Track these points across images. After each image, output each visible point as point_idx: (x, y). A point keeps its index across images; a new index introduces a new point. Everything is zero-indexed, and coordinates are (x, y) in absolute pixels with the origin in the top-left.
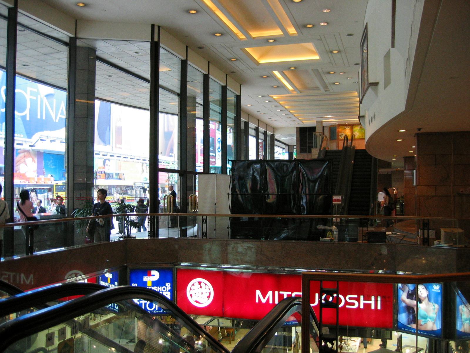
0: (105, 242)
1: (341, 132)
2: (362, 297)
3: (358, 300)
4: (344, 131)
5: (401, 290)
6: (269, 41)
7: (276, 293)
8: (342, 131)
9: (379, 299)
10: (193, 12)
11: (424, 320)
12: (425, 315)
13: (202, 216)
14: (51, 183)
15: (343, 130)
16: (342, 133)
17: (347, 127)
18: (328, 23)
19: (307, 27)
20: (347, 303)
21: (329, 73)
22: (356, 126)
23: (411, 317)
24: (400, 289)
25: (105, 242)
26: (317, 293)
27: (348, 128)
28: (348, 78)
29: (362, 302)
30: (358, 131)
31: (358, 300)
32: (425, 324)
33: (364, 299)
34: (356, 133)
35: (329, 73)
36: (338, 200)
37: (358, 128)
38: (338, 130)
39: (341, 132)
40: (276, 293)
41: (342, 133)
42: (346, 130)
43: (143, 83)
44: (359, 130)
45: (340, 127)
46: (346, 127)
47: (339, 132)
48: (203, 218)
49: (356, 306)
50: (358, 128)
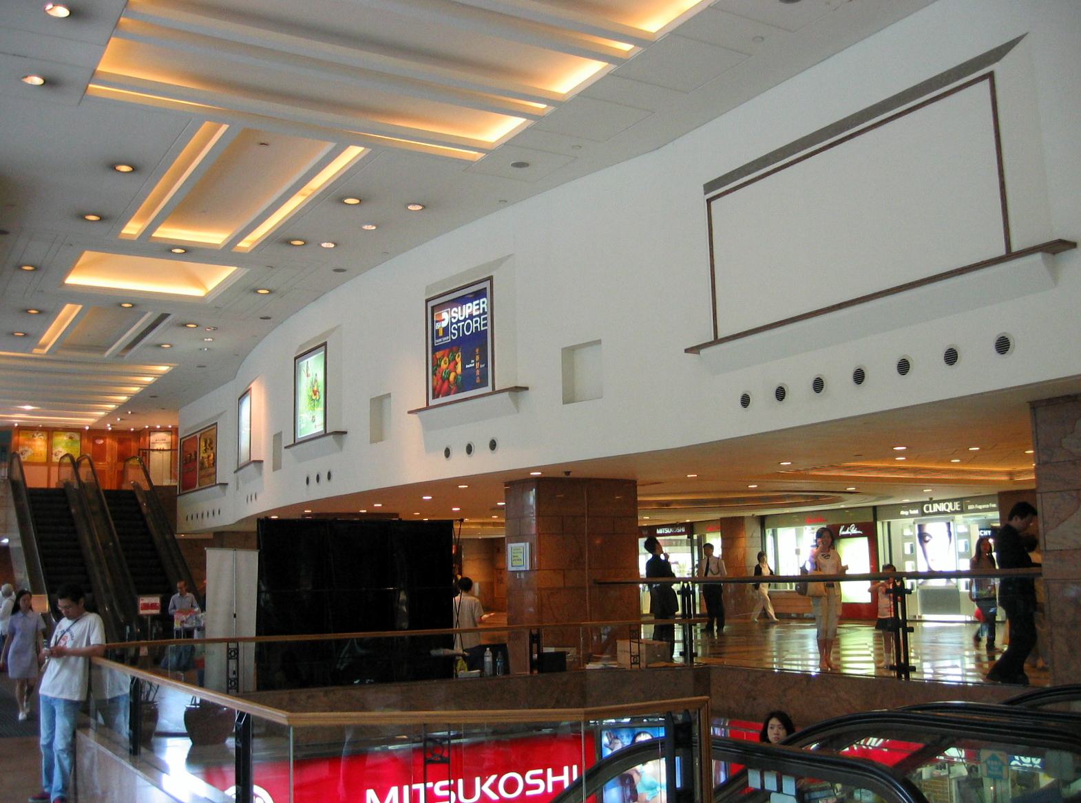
0: (663, 664)
1: (23, 445)
2: (550, 771)
3: (543, 777)
4: (30, 443)
5: (608, 749)
6: (184, 251)
7: (406, 788)
8: (27, 442)
9: (575, 768)
10: (124, 168)
11: (651, 792)
12: (653, 782)
13: (226, 644)
14: (932, 560)
15: (29, 440)
16: (26, 448)
17: (37, 433)
18: (336, 244)
19: (290, 243)
20: (527, 787)
21: (185, 325)
22: (60, 433)
23: (628, 793)
24: (606, 746)
25: (663, 664)
26: (406, 784)
27: (42, 437)
28: (206, 340)
29: (551, 779)
30: (64, 444)
31: (543, 777)
32: (653, 797)
33: (554, 774)
34: (60, 449)
35: (185, 325)
36: (153, 606)
37: (65, 438)
38: (15, 439)
39: (23, 445)
40: (406, 788)
41: (26, 448)
42: (34, 441)
43: (299, 350)
44: (67, 443)
45: (20, 432)
46: (35, 435)
47: (18, 445)
48: (230, 647)
49: (540, 791)
50: (65, 438)
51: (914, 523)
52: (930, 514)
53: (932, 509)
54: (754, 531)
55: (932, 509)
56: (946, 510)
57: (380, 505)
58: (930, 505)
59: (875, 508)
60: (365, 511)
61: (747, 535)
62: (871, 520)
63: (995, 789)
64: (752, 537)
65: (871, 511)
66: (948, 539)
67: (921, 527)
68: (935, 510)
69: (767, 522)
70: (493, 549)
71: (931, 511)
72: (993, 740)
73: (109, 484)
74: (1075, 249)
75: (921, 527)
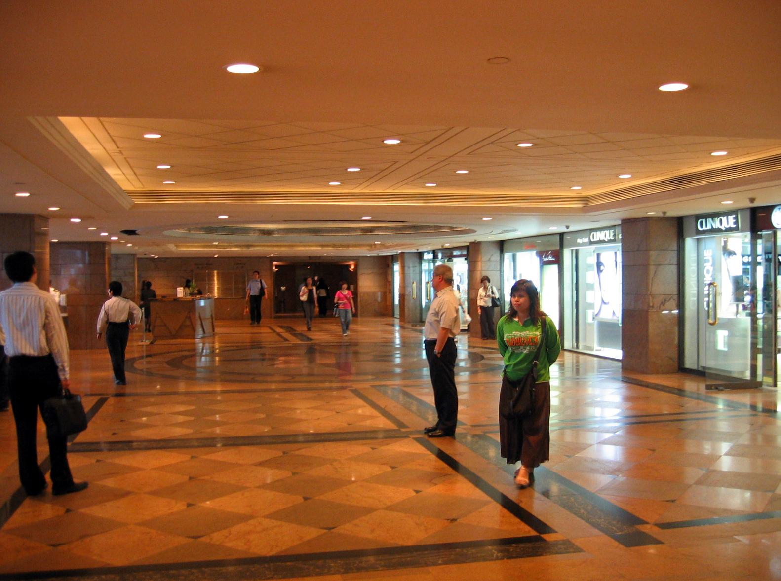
51: (594, 251)
52: (704, 232)
53: (706, 226)
54: (492, 255)
55: (706, 226)
56: (720, 227)
57: (27, 195)
58: (704, 220)
59: (562, 235)
60: (57, 241)
61: (483, 259)
62: (558, 248)
63: (354, 482)
64: (489, 261)
65: (558, 238)
66: (615, 269)
67: (598, 255)
68: (709, 227)
69: (506, 246)
70: (254, 567)
71: (705, 228)
72: (366, 432)
73: (469, 362)
74: (5, 348)
75: (598, 255)
